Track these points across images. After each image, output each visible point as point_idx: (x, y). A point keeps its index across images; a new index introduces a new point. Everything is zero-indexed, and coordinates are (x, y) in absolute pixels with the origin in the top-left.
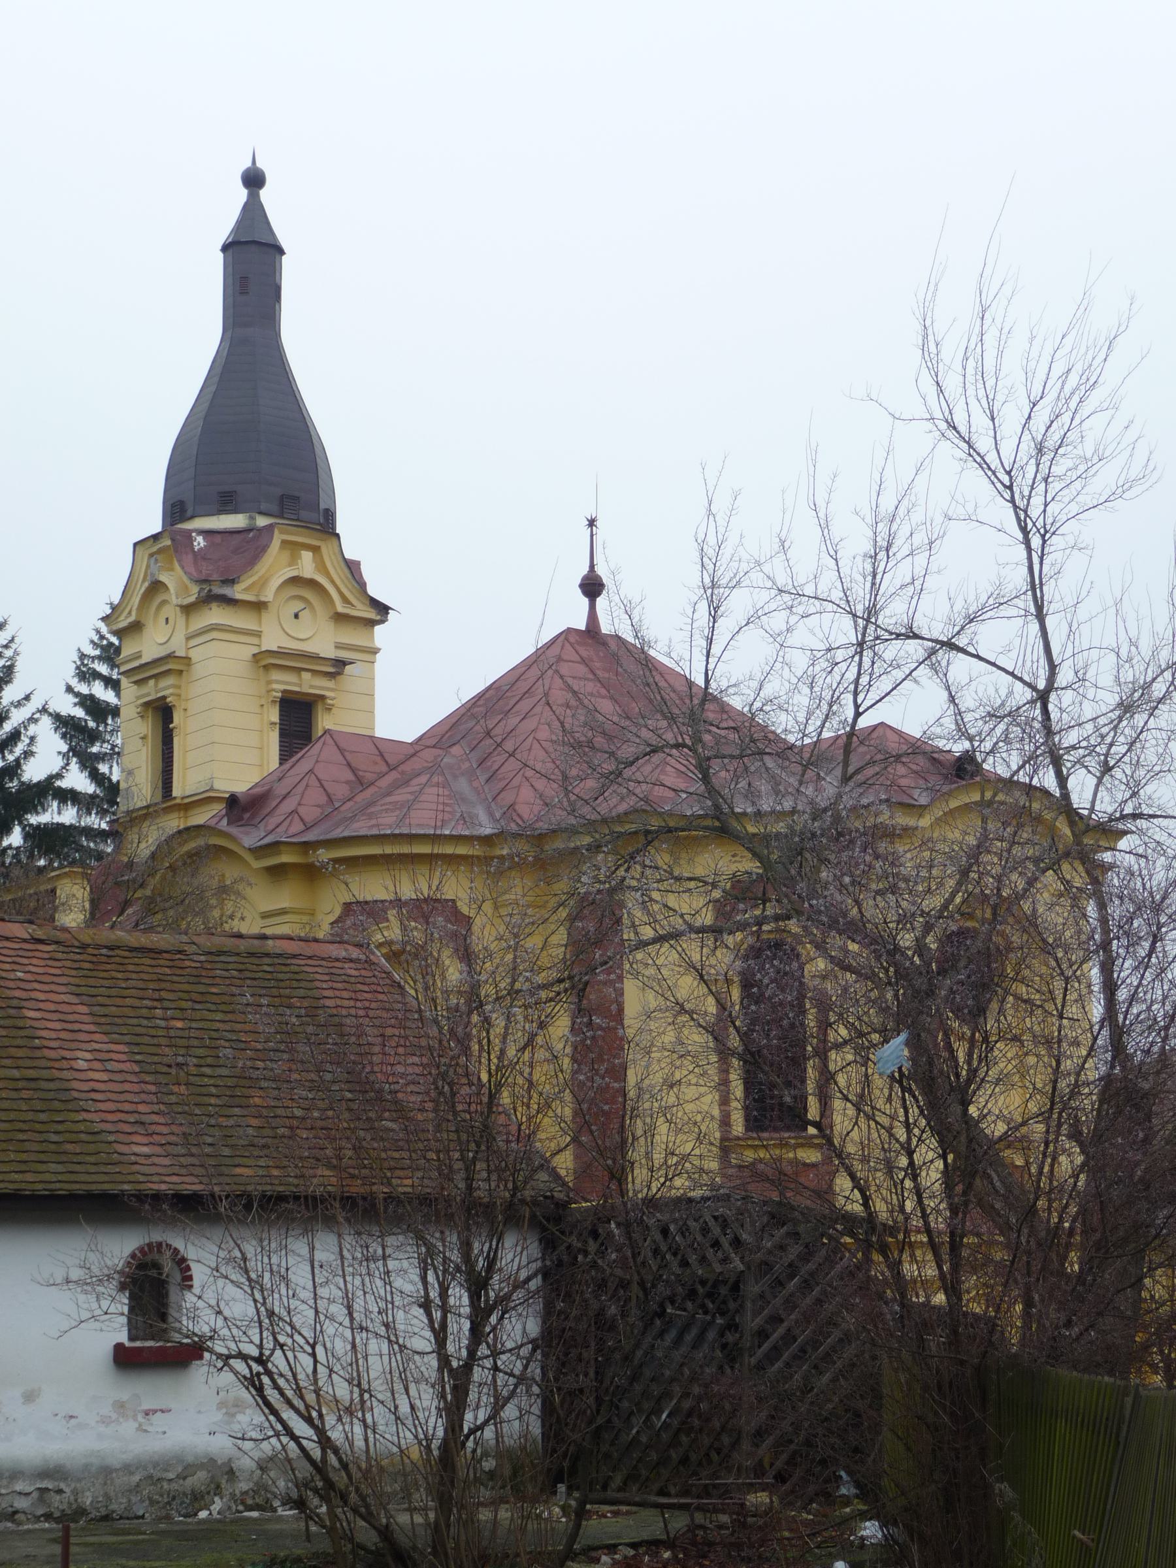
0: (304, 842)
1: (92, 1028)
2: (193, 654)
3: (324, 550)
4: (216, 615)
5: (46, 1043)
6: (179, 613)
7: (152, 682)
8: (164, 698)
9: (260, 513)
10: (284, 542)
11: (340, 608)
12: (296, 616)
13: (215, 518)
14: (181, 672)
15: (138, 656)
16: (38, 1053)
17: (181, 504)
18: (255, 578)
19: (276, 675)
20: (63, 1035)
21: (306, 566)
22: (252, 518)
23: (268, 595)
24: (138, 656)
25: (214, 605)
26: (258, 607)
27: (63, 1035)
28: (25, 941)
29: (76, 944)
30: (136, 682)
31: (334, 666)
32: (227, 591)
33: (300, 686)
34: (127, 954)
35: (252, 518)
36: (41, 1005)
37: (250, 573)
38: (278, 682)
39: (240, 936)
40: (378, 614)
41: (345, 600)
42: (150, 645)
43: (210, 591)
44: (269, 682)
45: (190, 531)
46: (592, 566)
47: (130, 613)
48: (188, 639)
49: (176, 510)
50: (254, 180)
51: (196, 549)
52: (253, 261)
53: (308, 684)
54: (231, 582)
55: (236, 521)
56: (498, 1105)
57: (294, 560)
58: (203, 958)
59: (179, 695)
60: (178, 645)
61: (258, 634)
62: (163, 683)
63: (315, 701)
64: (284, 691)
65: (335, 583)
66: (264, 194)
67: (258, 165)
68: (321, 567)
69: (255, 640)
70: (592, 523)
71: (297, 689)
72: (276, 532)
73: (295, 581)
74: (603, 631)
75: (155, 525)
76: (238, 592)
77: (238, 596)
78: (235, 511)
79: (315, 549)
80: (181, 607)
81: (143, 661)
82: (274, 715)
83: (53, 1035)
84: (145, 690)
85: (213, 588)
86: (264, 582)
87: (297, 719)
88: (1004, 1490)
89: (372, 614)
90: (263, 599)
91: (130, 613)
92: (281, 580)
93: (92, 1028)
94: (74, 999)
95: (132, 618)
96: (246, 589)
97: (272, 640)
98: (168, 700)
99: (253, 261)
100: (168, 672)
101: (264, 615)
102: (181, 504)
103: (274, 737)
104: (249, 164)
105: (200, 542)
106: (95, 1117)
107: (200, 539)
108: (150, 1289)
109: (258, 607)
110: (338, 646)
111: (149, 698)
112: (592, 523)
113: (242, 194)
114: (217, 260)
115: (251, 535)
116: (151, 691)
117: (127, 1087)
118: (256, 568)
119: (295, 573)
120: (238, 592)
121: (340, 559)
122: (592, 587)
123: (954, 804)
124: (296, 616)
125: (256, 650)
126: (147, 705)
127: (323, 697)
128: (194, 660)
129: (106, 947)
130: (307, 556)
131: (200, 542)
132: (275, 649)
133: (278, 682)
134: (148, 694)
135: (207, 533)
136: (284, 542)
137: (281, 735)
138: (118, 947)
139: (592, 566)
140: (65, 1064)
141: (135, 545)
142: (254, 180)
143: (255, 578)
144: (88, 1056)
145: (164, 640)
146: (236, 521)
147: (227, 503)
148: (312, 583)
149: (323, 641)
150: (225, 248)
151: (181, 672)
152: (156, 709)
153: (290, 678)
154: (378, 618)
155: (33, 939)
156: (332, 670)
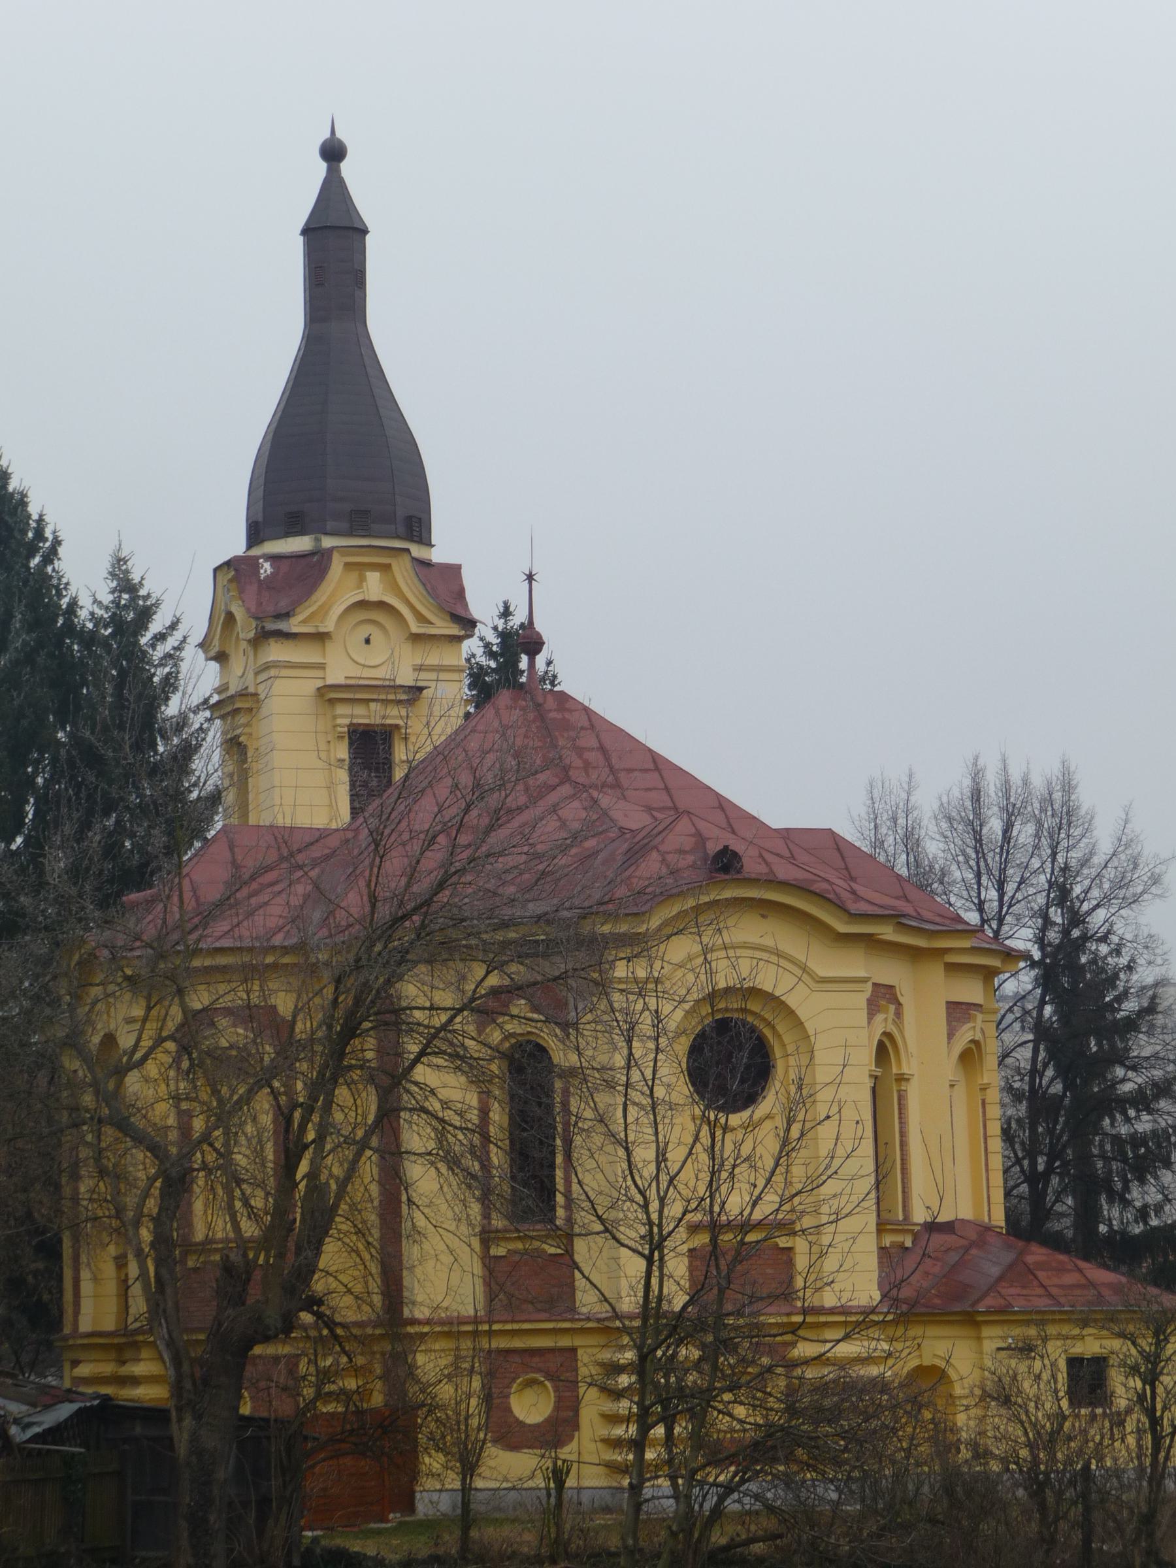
3: (395, 567)
4: (276, 652)
9: (326, 534)
10: (347, 564)
11: (415, 628)
12: (368, 641)
13: (283, 541)
14: (250, 710)
18: (311, 610)
19: (341, 709)
22: (318, 540)
23: (329, 626)
25: (272, 641)
26: (321, 638)
31: (404, 692)
32: (282, 626)
33: (369, 717)
35: (318, 540)
37: (307, 604)
38: (342, 716)
40: (463, 629)
41: (421, 618)
43: (263, 627)
44: (335, 717)
45: (258, 558)
48: (257, 674)
50: (333, 152)
51: (262, 577)
52: (334, 244)
54: (287, 615)
55: (300, 544)
56: (189, 1247)
59: (251, 734)
60: (250, 682)
61: (321, 667)
66: (345, 167)
67: (339, 135)
69: (319, 673)
70: (530, 578)
73: (362, 604)
76: (294, 625)
77: (295, 630)
78: (302, 532)
82: (342, 751)
85: (265, 624)
86: (324, 610)
87: (369, 748)
89: (455, 630)
96: (304, 622)
97: (335, 676)
98: (241, 739)
99: (334, 244)
103: (343, 776)
104: (327, 135)
105: (267, 568)
107: (267, 565)
109: (321, 638)
112: (530, 578)
113: (323, 166)
114: (298, 244)
115: (315, 558)
118: (314, 598)
119: (359, 598)
120: (294, 625)
123: (705, 899)
125: (320, 683)
130: (373, 577)
131: (267, 568)
132: (342, 681)
133: (342, 716)
135: (274, 558)
136: (347, 564)
141: (215, 570)
142: (333, 152)
146: (300, 544)
147: (295, 525)
148: (381, 605)
150: (305, 232)
153: (359, 710)
154: (462, 633)
156: (404, 697)
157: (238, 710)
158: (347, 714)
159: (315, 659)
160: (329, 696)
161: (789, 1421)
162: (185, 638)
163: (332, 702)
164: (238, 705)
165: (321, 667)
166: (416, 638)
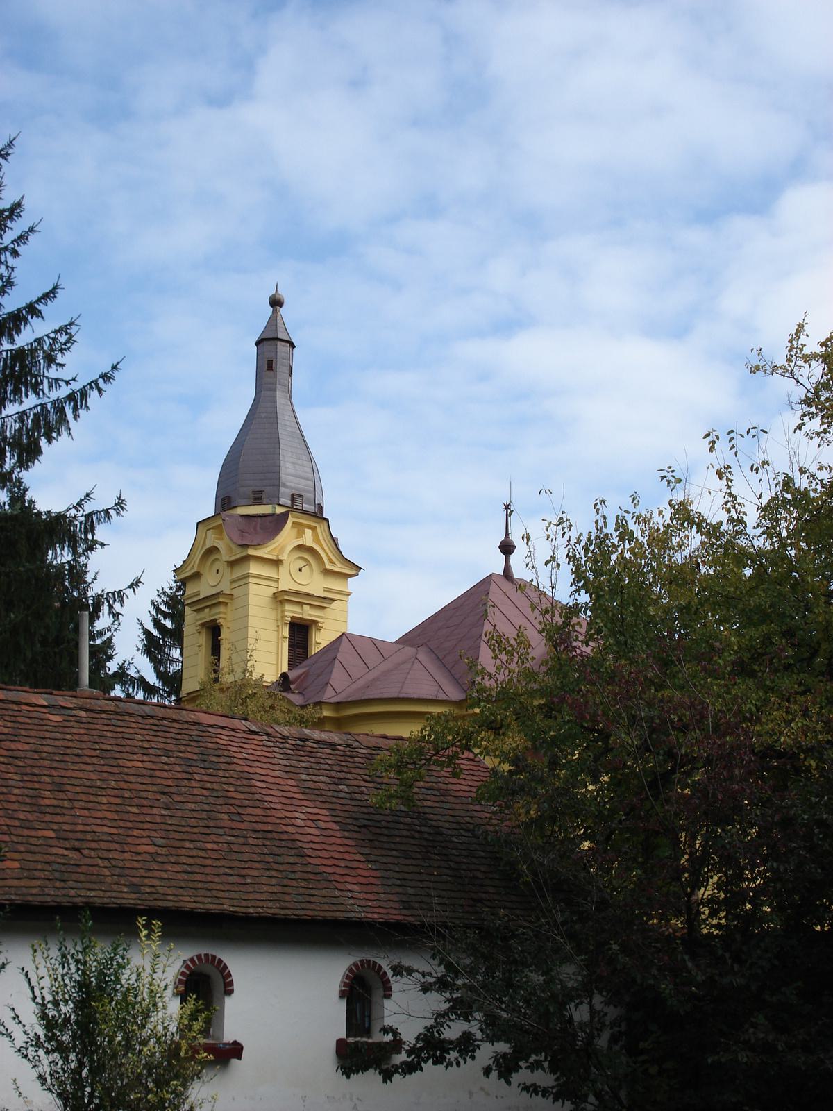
0: (338, 703)
1: (302, 797)
2: (234, 592)
5: (273, 806)
6: (226, 566)
7: (207, 610)
8: (216, 620)
11: (328, 566)
12: (300, 570)
15: (198, 594)
16: (269, 812)
17: (228, 498)
18: (274, 546)
19: (288, 607)
20: (283, 800)
21: (308, 539)
23: (284, 557)
24: (198, 594)
27: (283, 800)
28: (244, 732)
29: (279, 736)
30: (195, 611)
34: (315, 745)
36: (263, 778)
37: (269, 544)
39: (385, 737)
41: (331, 562)
42: (204, 588)
46: (507, 534)
47: (193, 566)
49: (225, 502)
50: (276, 303)
52: (23, 197)
53: (308, 613)
57: (300, 534)
58: (364, 751)
61: (276, 580)
62: (215, 610)
63: (311, 625)
64: (292, 617)
65: (325, 551)
67: (279, 292)
68: (317, 540)
69: (275, 584)
71: (301, 616)
72: (290, 516)
73: (300, 548)
74: (515, 577)
75: (208, 509)
79: (313, 529)
80: (228, 562)
81: (201, 597)
83: (275, 800)
84: (201, 615)
86: (282, 549)
87: (300, 632)
88: (218, 1067)
90: (280, 558)
91: (193, 566)
92: (292, 546)
93: (302, 797)
94: (284, 775)
95: (195, 570)
97: (284, 586)
99: (23, 197)
100: (219, 603)
101: (281, 568)
102: (228, 498)
103: (285, 646)
106: (317, 862)
108: (361, 994)
109: (277, 563)
110: (326, 590)
111: (203, 621)
116: (207, 616)
117: (333, 840)
121: (328, 534)
122: (507, 548)
124: (300, 570)
125: (275, 591)
126: (203, 625)
127: (316, 622)
128: (235, 596)
129: (300, 739)
130: (308, 532)
134: (205, 618)
136: (294, 523)
137: (290, 645)
138: (308, 740)
139: (507, 534)
140: (287, 821)
141: (198, 524)
142: (276, 303)
143: (274, 546)
144: (303, 816)
145: (215, 584)
148: (311, 550)
149: (315, 584)
151: (226, 604)
152: (208, 628)
153: (297, 609)
155: (250, 731)
157: (219, 603)
158: (292, 611)
159: (274, 575)
160: (280, 599)
161: (478, 733)
162: (801, 326)
163: (282, 602)
164: (221, 600)
165: (276, 580)
166: (328, 572)
